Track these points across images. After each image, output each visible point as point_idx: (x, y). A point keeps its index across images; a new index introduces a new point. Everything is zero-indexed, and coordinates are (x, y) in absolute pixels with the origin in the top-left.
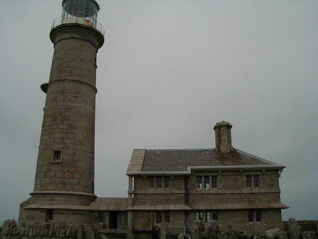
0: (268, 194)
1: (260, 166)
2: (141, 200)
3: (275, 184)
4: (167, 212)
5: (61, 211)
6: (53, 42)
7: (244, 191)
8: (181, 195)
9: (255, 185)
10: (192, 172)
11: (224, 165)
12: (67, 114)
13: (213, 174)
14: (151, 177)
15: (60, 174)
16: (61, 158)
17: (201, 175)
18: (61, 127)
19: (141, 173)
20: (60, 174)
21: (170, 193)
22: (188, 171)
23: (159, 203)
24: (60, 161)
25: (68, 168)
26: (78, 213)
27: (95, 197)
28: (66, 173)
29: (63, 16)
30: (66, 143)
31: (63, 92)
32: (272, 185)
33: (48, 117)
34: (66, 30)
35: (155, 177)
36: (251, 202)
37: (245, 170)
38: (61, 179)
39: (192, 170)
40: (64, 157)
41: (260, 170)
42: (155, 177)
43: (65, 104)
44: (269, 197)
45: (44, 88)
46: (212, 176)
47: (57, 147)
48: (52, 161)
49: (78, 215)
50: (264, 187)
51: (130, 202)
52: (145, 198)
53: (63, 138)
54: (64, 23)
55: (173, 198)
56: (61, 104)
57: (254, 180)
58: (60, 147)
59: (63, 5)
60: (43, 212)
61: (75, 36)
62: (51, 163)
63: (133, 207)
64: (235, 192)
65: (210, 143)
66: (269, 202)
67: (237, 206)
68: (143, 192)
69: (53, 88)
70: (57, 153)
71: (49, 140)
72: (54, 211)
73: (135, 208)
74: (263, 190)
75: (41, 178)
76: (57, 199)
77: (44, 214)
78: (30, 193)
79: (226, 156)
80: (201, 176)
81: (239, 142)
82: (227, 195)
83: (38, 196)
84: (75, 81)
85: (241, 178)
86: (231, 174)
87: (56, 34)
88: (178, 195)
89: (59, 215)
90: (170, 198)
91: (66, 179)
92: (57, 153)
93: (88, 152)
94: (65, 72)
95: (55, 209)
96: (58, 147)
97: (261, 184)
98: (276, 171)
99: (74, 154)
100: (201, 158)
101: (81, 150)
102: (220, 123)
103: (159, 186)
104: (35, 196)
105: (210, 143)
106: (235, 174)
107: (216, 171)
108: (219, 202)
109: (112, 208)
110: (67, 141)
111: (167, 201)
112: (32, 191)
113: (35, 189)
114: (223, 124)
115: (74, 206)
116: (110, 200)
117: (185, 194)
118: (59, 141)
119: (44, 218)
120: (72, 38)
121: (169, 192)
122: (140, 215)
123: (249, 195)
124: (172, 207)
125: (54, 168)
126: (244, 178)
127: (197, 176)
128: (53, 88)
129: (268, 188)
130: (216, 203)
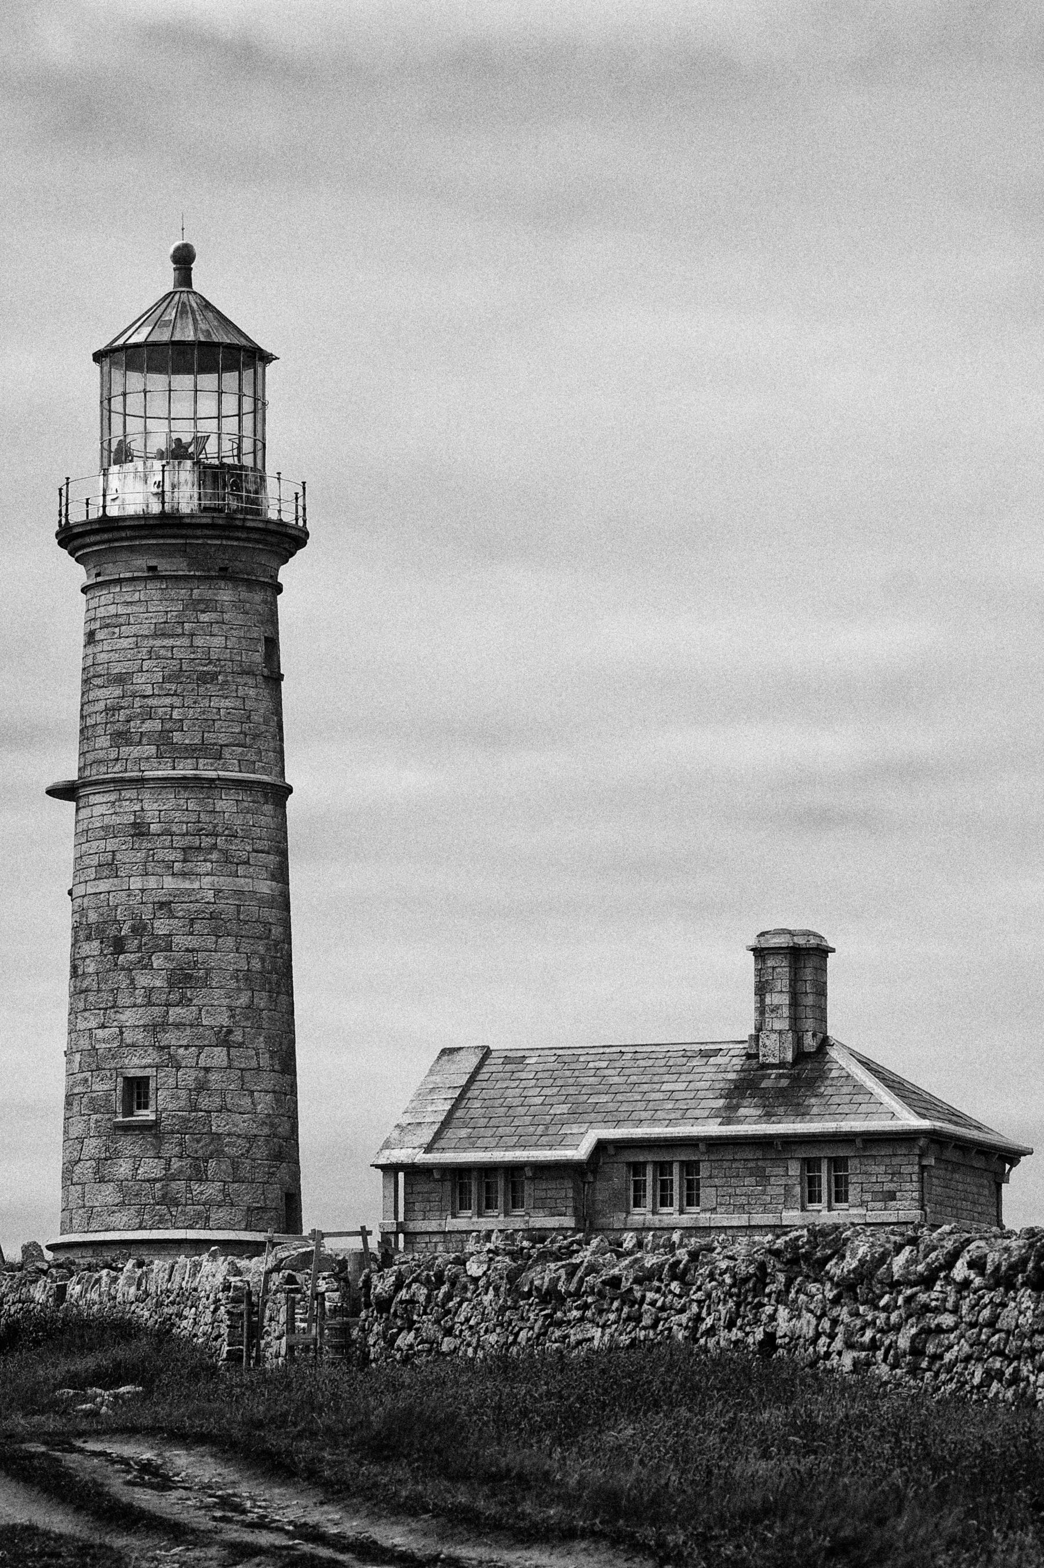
14: (459, 1173)
15: (151, 1168)
16: (152, 1102)
18: (143, 980)
19: (421, 1157)
20: (151, 1168)
22: (580, 1152)
24: (147, 1115)
28: (176, 1164)
30: (169, 1047)
31: (139, 830)
32: (891, 1196)
33: (88, 938)
34: (122, 539)
35: (475, 1174)
37: (790, 1141)
38: (158, 1185)
40: (164, 1102)
42: (475, 1174)
47: (135, 1065)
50: (863, 1204)
53: (155, 1026)
56: (136, 883)
58: (148, 1061)
61: (165, 566)
64: (758, 1219)
65: (722, 1008)
68: (432, 1226)
69: (98, 810)
70: (136, 1091)
71: (100, 1033)
78: (50, 782)
84: (183, 783)
85: (781, 1171)
92: (136, 1091)
93: (259, 1069)
94: (140, 743)
96: (136, 1061)
99: (202, 1087)
101: (230, 1067)
106: (759, 1154)
110: (169, 1038)
118: (139, 1036)
125: (127, 1145)
126: (795, 1169)
128: (98, 810)
129: (880, 1205)
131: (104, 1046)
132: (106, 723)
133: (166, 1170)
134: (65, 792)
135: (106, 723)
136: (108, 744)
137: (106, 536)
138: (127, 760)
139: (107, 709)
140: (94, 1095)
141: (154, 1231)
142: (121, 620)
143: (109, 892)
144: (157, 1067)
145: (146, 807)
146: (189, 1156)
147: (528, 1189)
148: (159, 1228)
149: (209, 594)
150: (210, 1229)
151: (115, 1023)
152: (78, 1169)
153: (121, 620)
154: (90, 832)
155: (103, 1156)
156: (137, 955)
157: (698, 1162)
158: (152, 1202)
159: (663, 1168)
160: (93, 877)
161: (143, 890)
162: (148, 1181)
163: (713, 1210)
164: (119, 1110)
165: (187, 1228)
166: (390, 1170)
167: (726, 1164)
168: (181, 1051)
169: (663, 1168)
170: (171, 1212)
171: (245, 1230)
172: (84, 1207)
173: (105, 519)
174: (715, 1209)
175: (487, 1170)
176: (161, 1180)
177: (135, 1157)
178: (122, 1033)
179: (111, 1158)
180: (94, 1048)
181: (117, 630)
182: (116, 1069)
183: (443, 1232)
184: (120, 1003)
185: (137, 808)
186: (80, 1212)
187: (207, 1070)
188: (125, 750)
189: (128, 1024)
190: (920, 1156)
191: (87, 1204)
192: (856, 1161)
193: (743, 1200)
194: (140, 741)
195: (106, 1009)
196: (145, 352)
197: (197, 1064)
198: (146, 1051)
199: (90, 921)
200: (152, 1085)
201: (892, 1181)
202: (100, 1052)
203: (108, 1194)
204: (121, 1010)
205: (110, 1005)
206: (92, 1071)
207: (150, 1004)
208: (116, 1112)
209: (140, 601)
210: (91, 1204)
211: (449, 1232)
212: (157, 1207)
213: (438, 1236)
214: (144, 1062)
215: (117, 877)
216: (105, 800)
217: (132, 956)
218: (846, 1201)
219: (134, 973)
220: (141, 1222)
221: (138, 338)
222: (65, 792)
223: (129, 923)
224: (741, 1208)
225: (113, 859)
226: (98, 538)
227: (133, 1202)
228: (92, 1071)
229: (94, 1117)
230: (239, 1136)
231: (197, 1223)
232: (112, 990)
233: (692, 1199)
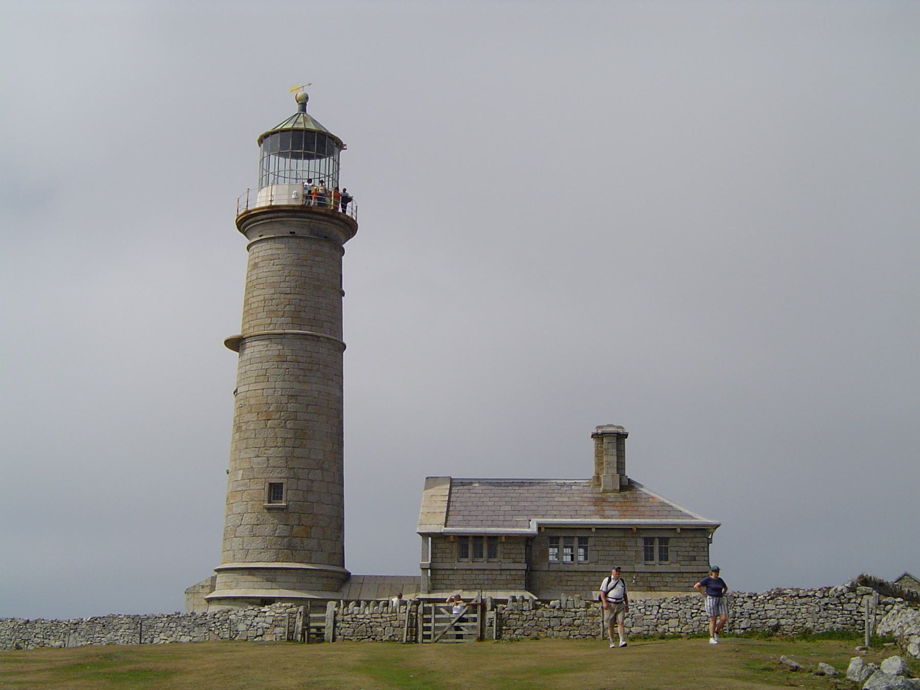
0: (685, 575)
1: (670, 521)
7: (640, 567)
8: (519, 573)
10: (539, 529)
11: (604, 517)
14: (462, 539)
19: (443, 529)
22: (533, 529)
27: (348, 575)
28: (296, 529)
32: (694, 559)
39: (540, 527)
41: (672, 529)
48: (266, 504)
51: (425, 584)
54: (273, 204)
55: (504, 577)
57: (660, 548)
61: (299, 232)
65: (581, 464)
68: (448, 566)
74: (675, 567)
80: (558, 538)
86: (616, 534)
88: (513, 573)
90: (499, 577)
97: (671, 556)
98: (704, 532)
99: (310, 490)
100: (562, 499)
101: (323, 481)
107: (587, 528)
117: (526, 571)
123: (648, 575)
126: (641, 543)
127: (551, 538)
129: (687, 563)
134: (235, 344)
139: (265, 300)
147: (499, 548)
163: (597, 562)
166: (425, 535)
167: (603, 539)
173: (271, 207)
175: (478, 538)
187: (312, 481)
193: (613, 558)
196: (291, 133)
214: (280, 475)
218: (667, 560)
221: (289, 126)
222: (235, 344)
233: (664, 557)
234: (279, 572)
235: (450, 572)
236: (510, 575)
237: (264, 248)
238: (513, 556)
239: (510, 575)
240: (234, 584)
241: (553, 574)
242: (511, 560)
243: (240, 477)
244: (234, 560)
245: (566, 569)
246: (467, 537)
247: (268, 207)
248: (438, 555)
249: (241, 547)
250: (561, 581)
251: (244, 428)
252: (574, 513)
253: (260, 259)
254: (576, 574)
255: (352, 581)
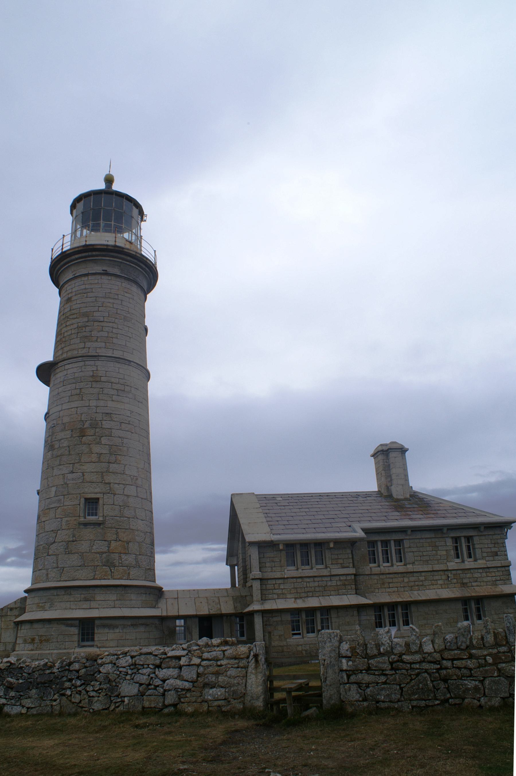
0: (491, 570)
2: (275, 591)
3: (499, 551)
4: (327, 610)
5: (110, 622)
6: (58, 288)
7: (453, 565)
8: (349, 578)
9: (316, 560)
12: (106, 424)
13: (383, 538)
15: (100, 546)
17: (376, 539)
18: (96, 449)
20: (100, 546)
21: (328, 574)
23: (313, 593)
25: (117, 534)
26: (143, 624)
28: (113, 544)
29: (74, 232)
30: (110, 483)
32: (496, 554)
36: (464, 585)
38: (104, 555)
40: (106, 510)
41: (476, 527)
42: (298, 546)
43: (102, 403)
44: (493, 574)
45: (45, 372)
46: (395, 541)
48: (82, 519)
49: (142, 629)
50: (483, 558)
52: (282, 587)
54: (87, 243)
56: (93, 403)
59: (72, 213)
60: (72, 626)
61: (111, 270)
62: (80, 524)
63: (262, 604)
64: (437, 567)
65: (367, 481)
66: (494, 583)
67: (445, 593)
68: (278, 575)
70: (92, 504)
71: (70, 476)
72: (97, 622)
73: (269, 605)
74: (481, 563)
75: (57, 555)
76: (98, 597)
77: (75, 630)
79: (406, 504)
81: (425, 478)
82: (423, 574)
83: (55, 592)
87: (60, 268)
89: (106, 630)
91: (112, 555)
92: (92, 504)
94: (97, 341)
95: (100, 618)
102: (386, 445)
103: (306, 562)
104: (33, 594)
105: (367, 481)
107: (403, 530)
108: (411, 588)
109: (204, 611)
111: (324, 591)
112: (28, 585)
113: (35, 580)
114: (394, 446)
115: (124, 610)
116: (195, 595)
119: (76, 638)
120: (106, 273)
121: (326, 572)
122: (275, 619)
124: (335, 601)
125: (88, 533)
126: (450, 542)
129: (491, 558)
130: (406, 589)
131: (73, 482)
132: (78, 333)
133: (109, 547)
135: (78, 333)
136: (79, 341)
137: (83, 255)
138: (89, 348)
139: (78, 327)
140: (65, 507)
141: (102, 580)
142: (88, 291)
143: (77, 408)
144: (104, 493)
145: (99, 369)
146: (120, 540)
147: (328, 554)
148: (105, 579)
149: (128, 286)
150: (131, 580)
151: (80, 471)
152: (53, 547)
153: (88, 291)
154: (65, 382)
155: (71, 539)
156: (93, 437)
157: (402, 540)
158: (101, 564)
159: (386, 543)
160: (67, 401)
161: (97, 407)
162: (98, 553)
164: (82, 514)
165: (119, 579)
167: (416, 541)
168: (116, 486)
169: (386, 543)
170: (111, 570)
171: (145, 580)
172: (57, 567)
173: (86, 245)
174: (414, 563)
176: (106, 553)
177: (91, 540)
178: (84, 475)
179: (76, 541)
180: (66, 484)
181: (85, 295)
182: (80, 494)
183: (284, 578)
184: (82, 461)
185: (95, 369)
186: (54, 570)
188: (88, 344)
189: (87, 471)
190: (115, 566)
191: (60, 566)
192: (477, 537)
193: (427, 558)
194: (97, 340)
195: (74, 464)
197: (123, 493)
198: (97, 485)
199: (64, 421)
200: (101, 502)
201: (495, 547)
202: (69, 485)
203: (75, 560)
204: (83, 464)
205: (76, 461)
206: (64, 495)
207: (100, 461)
208: (79, 516)
209: (98, 283)
210: (63, 566)
211: (287, 578)
212: (104, 567)
213: (441, 572)
215: (82, 400)
216: (76, 366)
217: (90, 437)
219: (91, 446)
220: (95, 575)
223: (89, 422)
224: (427, 562)
225: (80, 392)
226: (80, 255)
227: (90, 564)
228: (64, 495)
229: (65, 520)
230: (141, 531)
231: (124, 576)
232: (79, 454)
234: (97, 591)
235: (280, 581)
236: (340, 580)
237: (77, 284)
238: (341, 561)
239: (340, 580)
240: (47, 605)
241: (376, 577)
242: (339, 566)
243: (53, 494)
244: (47, 580)
245: (387, 572)
246: (310, 544)
247: (83, 246)
248: (268, 565)
249: (55, 565)
250: (383, 584)
251: (56, 446)
252: (384, 518)
253: (74, 294)
254: (396, 575)
255: (167, 595)
